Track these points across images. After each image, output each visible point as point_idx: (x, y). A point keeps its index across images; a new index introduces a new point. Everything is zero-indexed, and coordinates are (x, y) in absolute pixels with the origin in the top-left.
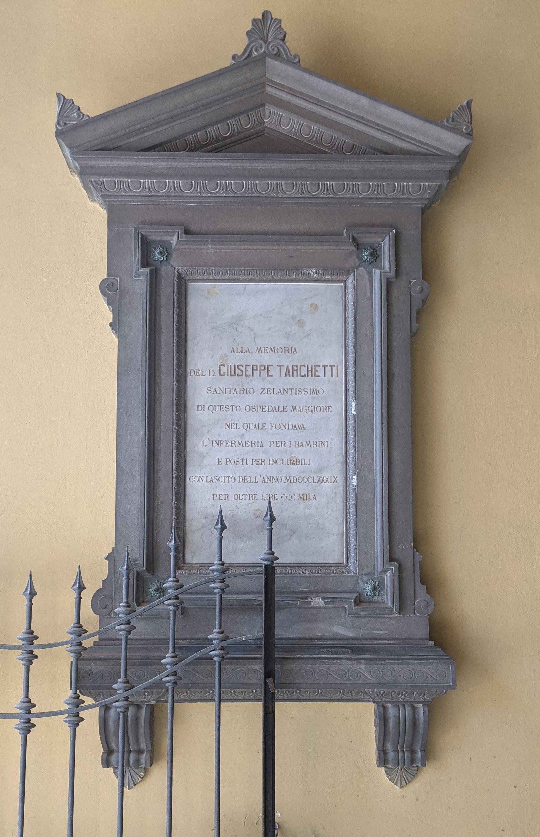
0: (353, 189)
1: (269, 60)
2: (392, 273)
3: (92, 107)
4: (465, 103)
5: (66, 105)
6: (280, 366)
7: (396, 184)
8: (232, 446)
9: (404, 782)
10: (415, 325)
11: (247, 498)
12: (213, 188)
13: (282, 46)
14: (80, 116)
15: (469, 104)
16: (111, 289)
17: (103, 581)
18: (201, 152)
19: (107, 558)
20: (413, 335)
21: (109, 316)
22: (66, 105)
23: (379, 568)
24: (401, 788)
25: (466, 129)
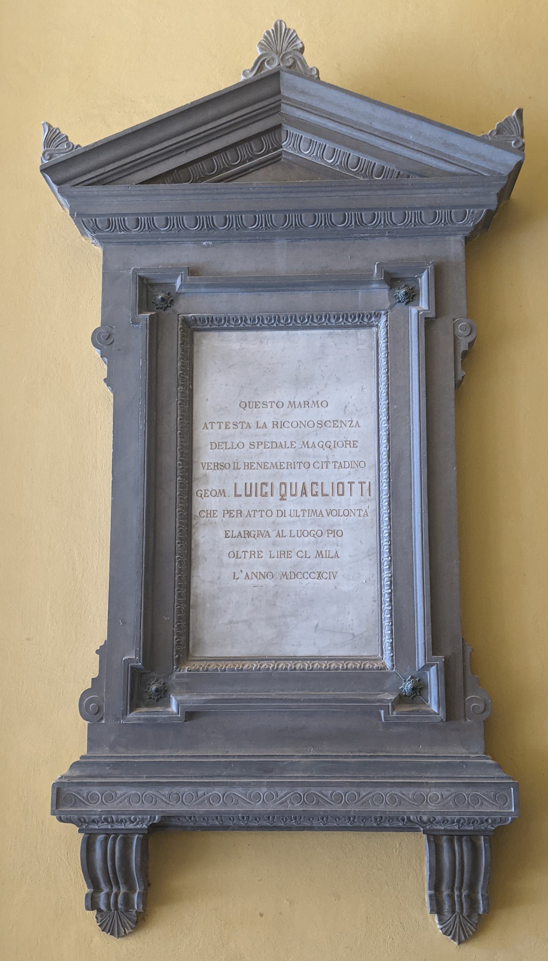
0: (178, 225)
1: (286, 77)
2: (432, 315)
3: (84, 136)
4: (514, 113)
5: (53, 137)
6: (361, 483)
7: (346, 214)
8: (214, 469)
9: (463, 938)
10: (461, 373)
11: (248, 555)
12: (105, 227)
13: (300, 59)
14: (69, 146)
15: (520, 113)
16: (104, 339)
17: (93, 680)
18: (208, 182)
19: (97, 652)
20: (458, 385)
21: (102, 369)
22: (53, 137)
23: (421, 662)
24: (459, 943)
25: (515, 144)
